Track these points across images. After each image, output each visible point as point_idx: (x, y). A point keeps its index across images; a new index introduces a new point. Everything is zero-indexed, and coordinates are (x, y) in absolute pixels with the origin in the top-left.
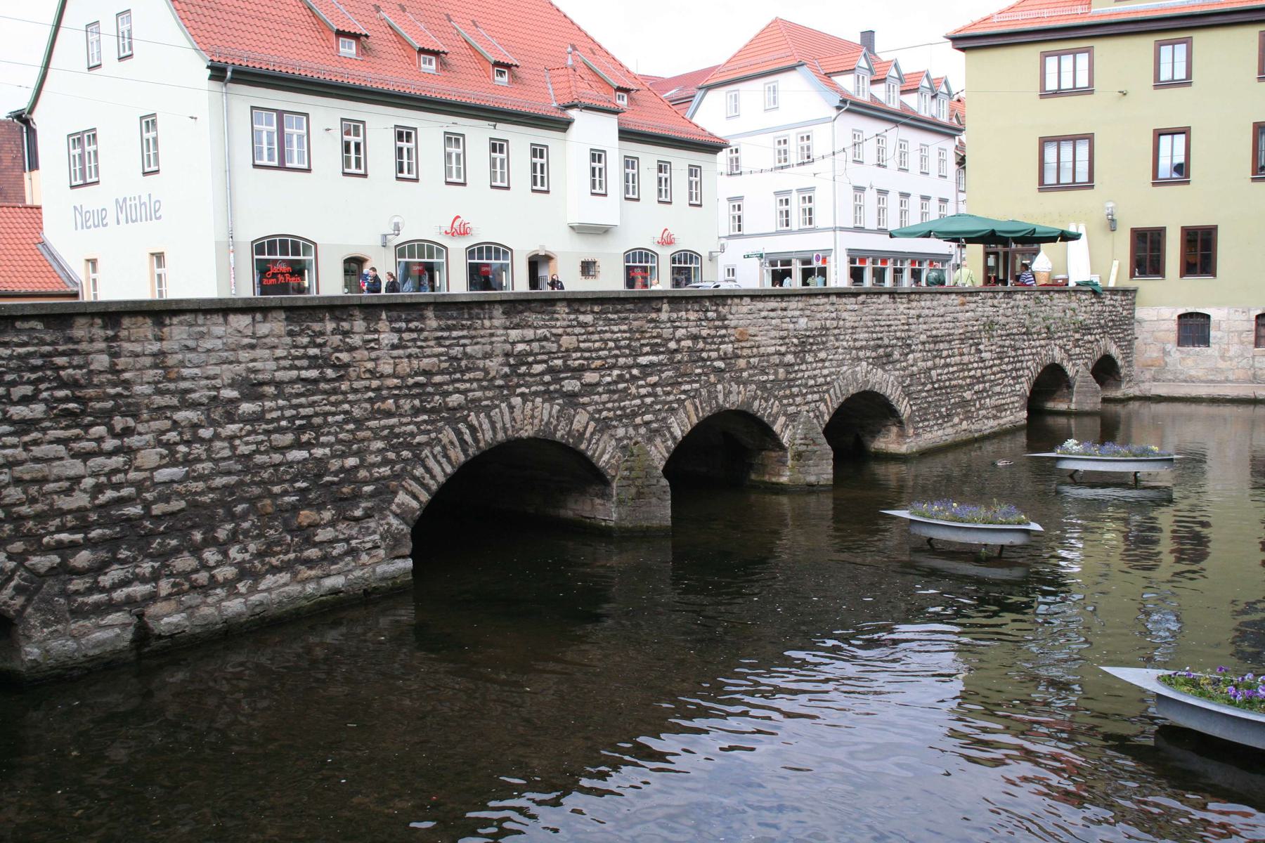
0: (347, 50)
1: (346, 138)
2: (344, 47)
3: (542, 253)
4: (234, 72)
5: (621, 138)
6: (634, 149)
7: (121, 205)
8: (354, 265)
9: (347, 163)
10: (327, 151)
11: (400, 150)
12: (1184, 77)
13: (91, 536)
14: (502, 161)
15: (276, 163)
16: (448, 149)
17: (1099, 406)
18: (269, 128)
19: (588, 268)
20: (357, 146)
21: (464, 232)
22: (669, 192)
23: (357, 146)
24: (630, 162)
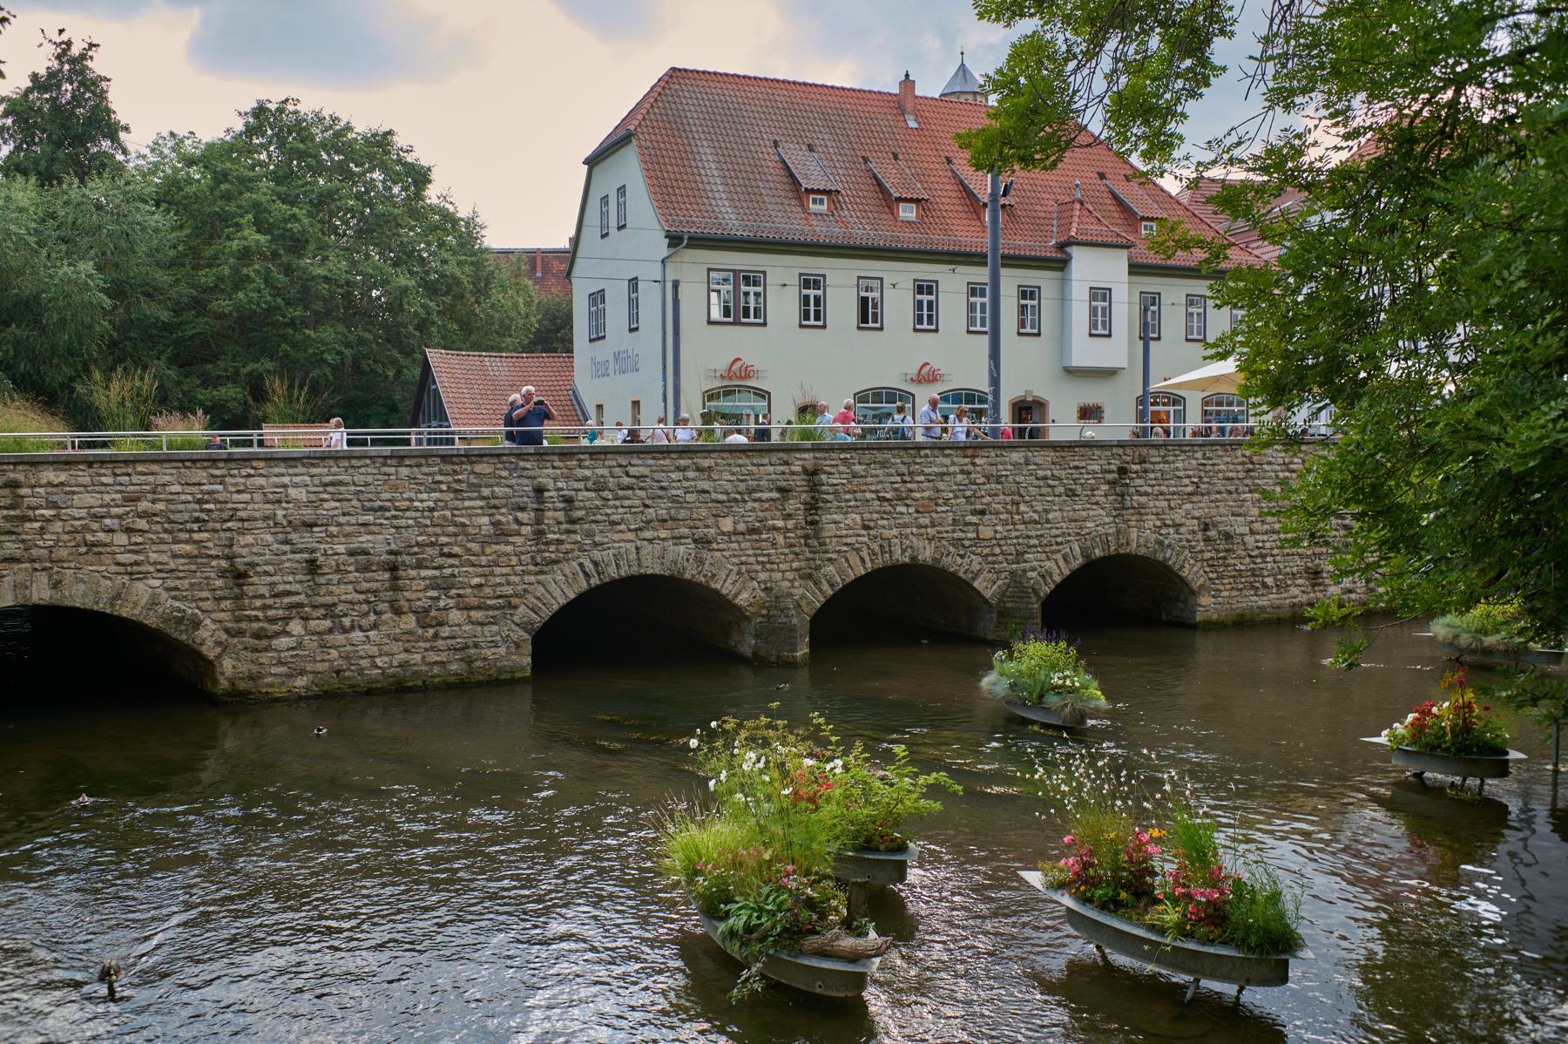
0: (908, 215)
1: (1023, 302)
2: (905, 211)
3: (1029, 399)
4: (689, 239)
5: (1130, 273)
6: (1152, 284)
7: (617, 356)
8: (808, 410)
9: (920, 320)
10: (783, 304)
11: (920, 303)
12: (917, 93)
13: (1427, 775)
14: (1104, 309)
15: (731, 320)
16: (1190, 310)
17: (345, 448)
18: (983, 300)
19: (1089, 413)
20: (817, 300)
21: (932, 378)
22: (1107, 324)
23: (817, 300)
24: (1150, 302)
